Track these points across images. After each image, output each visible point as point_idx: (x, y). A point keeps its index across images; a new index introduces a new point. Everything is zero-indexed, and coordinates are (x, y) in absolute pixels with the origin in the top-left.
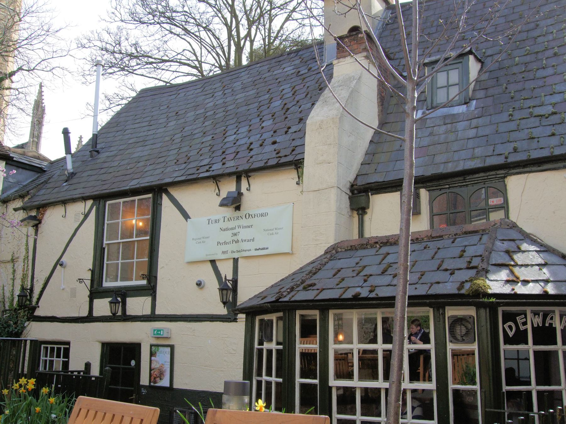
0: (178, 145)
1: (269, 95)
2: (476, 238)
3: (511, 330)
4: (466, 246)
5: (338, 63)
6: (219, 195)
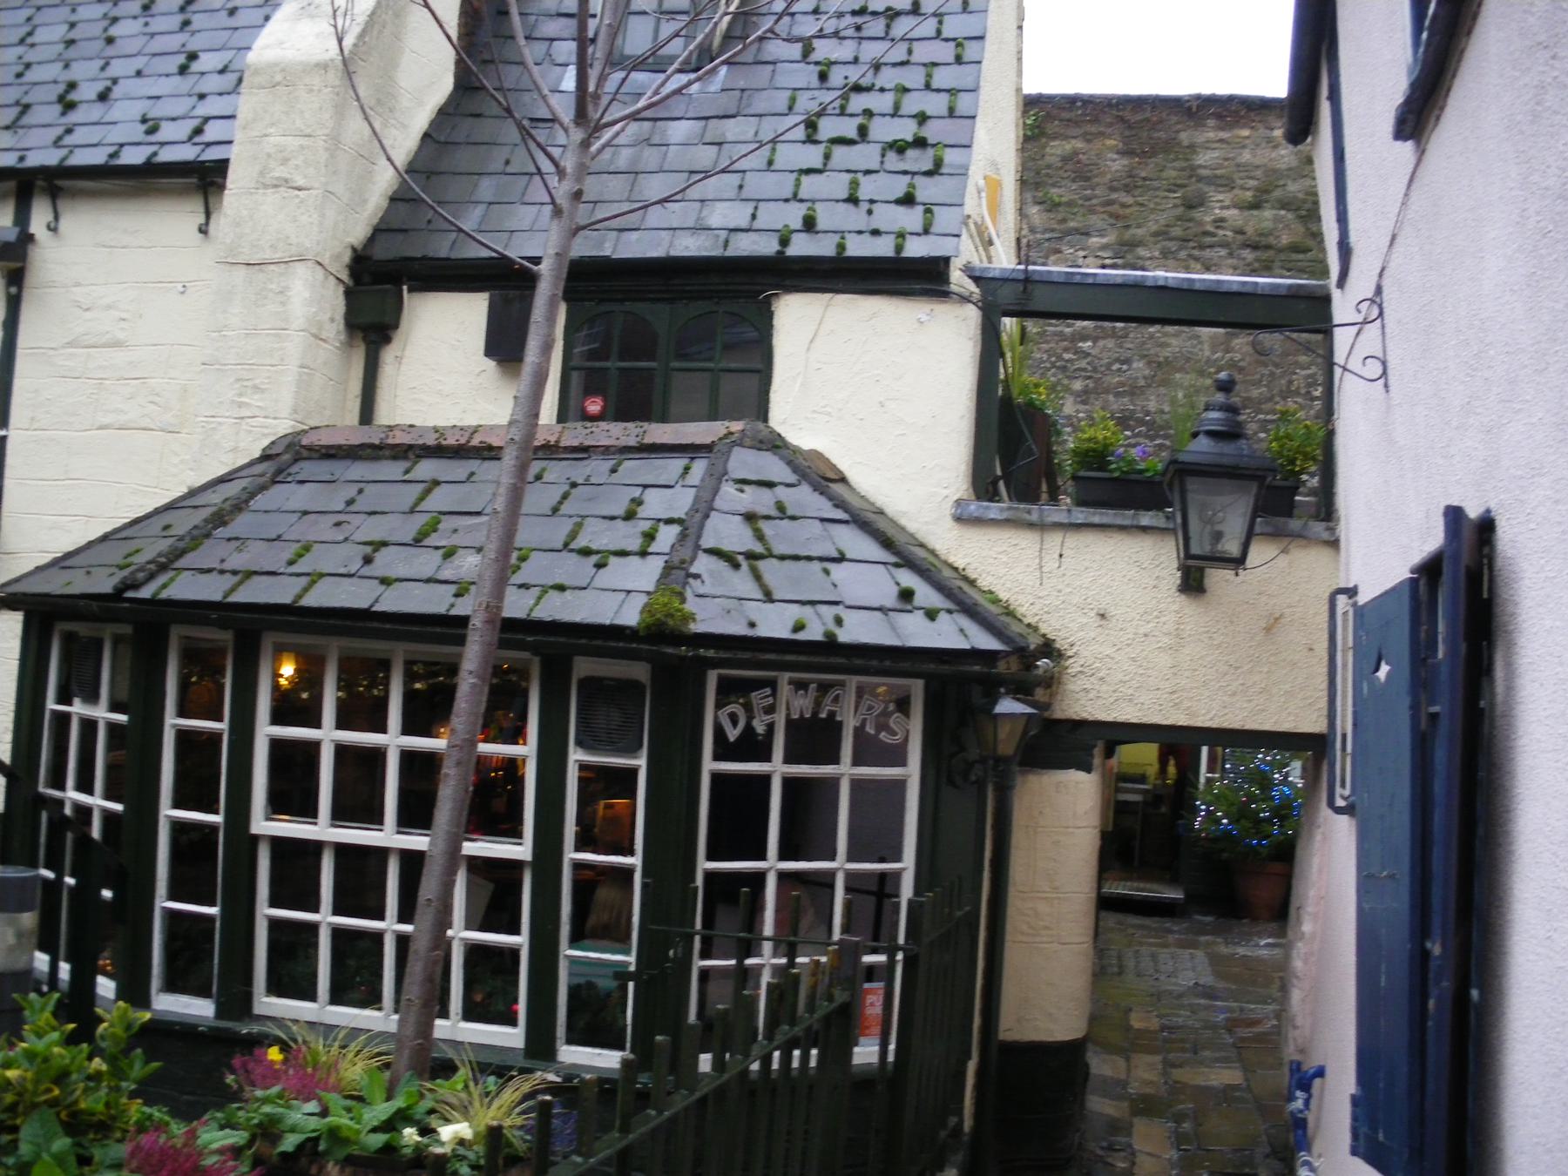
2: (676, 464)
3: (735, 723)
4: (645, 487)
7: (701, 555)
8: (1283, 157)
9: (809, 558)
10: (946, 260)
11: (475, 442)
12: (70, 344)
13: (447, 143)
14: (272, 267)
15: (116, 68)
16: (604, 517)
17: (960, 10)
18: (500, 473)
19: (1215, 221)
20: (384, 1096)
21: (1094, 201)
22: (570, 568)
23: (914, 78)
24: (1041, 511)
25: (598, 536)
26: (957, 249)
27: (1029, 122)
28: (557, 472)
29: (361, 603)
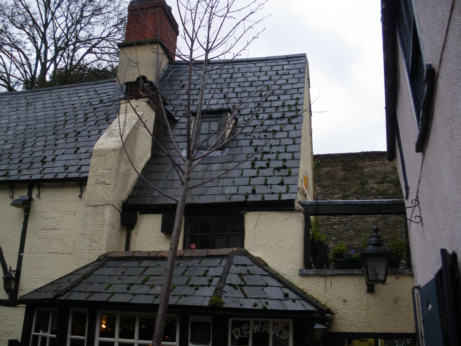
1: (65, 117)
2: (218, 261)
4: (209, 267)
7: (226, 285)
8: (388, 168)
9: (257, 286)
10: (293, 201)
11: (159, 256)
12: (41, 229)
13: (149, 172)
14: (100, 207)
15: (57, 152)
16: (197, 276)
17: (294, 129)
18: (167, 265)
19: (371, 188)
21: (335, 185)
22: (188, 290)
23: (282, 149)
24: (325, 271)
25: (196, 281)
26: (296, 197)
27: (315, 163)
28: (183, 263)
29: (127, 300)
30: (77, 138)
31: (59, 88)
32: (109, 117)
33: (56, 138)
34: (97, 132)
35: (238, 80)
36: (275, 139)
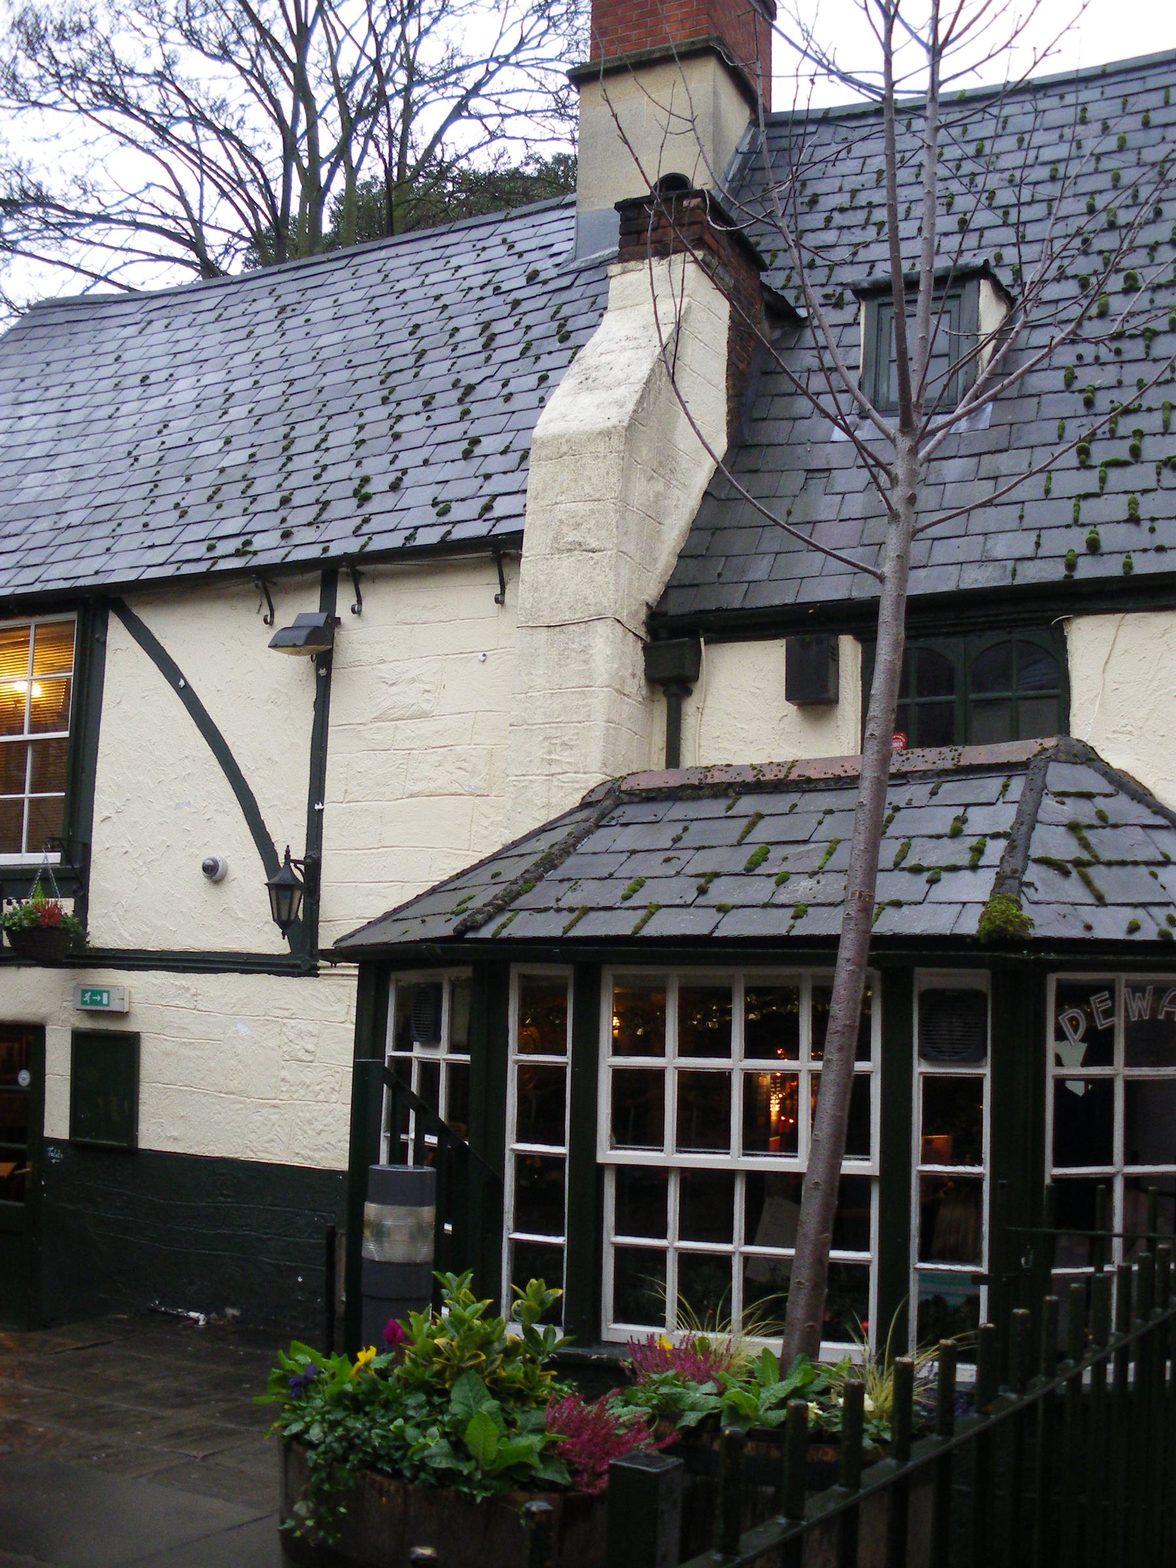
0: (149, 475)
2: (993, 785)
4: (967, 806)
5: (624, 272)
6: (271, 624)
9: (1135, 863)
11: (793, 776)
12: (377, 719)
13: (728, 499)
15: (404, 461)
16: (931, 837)
20: (778, 1377)
30: (466, 406)
31: (381, 248)
32: (569, 328)
33: (395, 414)
34: (533, 380)
35: (1004, 162)
36: (1155, 361)
